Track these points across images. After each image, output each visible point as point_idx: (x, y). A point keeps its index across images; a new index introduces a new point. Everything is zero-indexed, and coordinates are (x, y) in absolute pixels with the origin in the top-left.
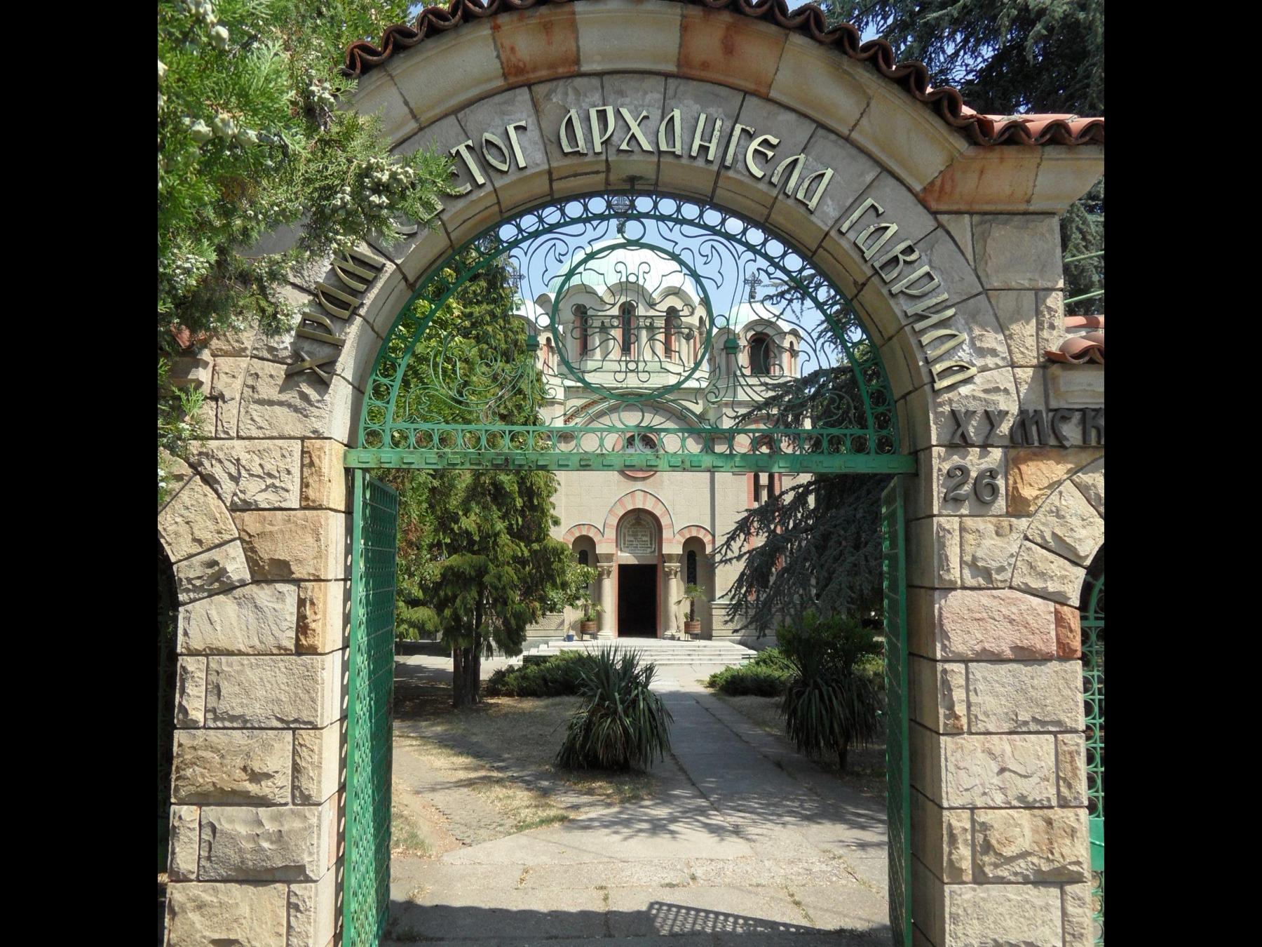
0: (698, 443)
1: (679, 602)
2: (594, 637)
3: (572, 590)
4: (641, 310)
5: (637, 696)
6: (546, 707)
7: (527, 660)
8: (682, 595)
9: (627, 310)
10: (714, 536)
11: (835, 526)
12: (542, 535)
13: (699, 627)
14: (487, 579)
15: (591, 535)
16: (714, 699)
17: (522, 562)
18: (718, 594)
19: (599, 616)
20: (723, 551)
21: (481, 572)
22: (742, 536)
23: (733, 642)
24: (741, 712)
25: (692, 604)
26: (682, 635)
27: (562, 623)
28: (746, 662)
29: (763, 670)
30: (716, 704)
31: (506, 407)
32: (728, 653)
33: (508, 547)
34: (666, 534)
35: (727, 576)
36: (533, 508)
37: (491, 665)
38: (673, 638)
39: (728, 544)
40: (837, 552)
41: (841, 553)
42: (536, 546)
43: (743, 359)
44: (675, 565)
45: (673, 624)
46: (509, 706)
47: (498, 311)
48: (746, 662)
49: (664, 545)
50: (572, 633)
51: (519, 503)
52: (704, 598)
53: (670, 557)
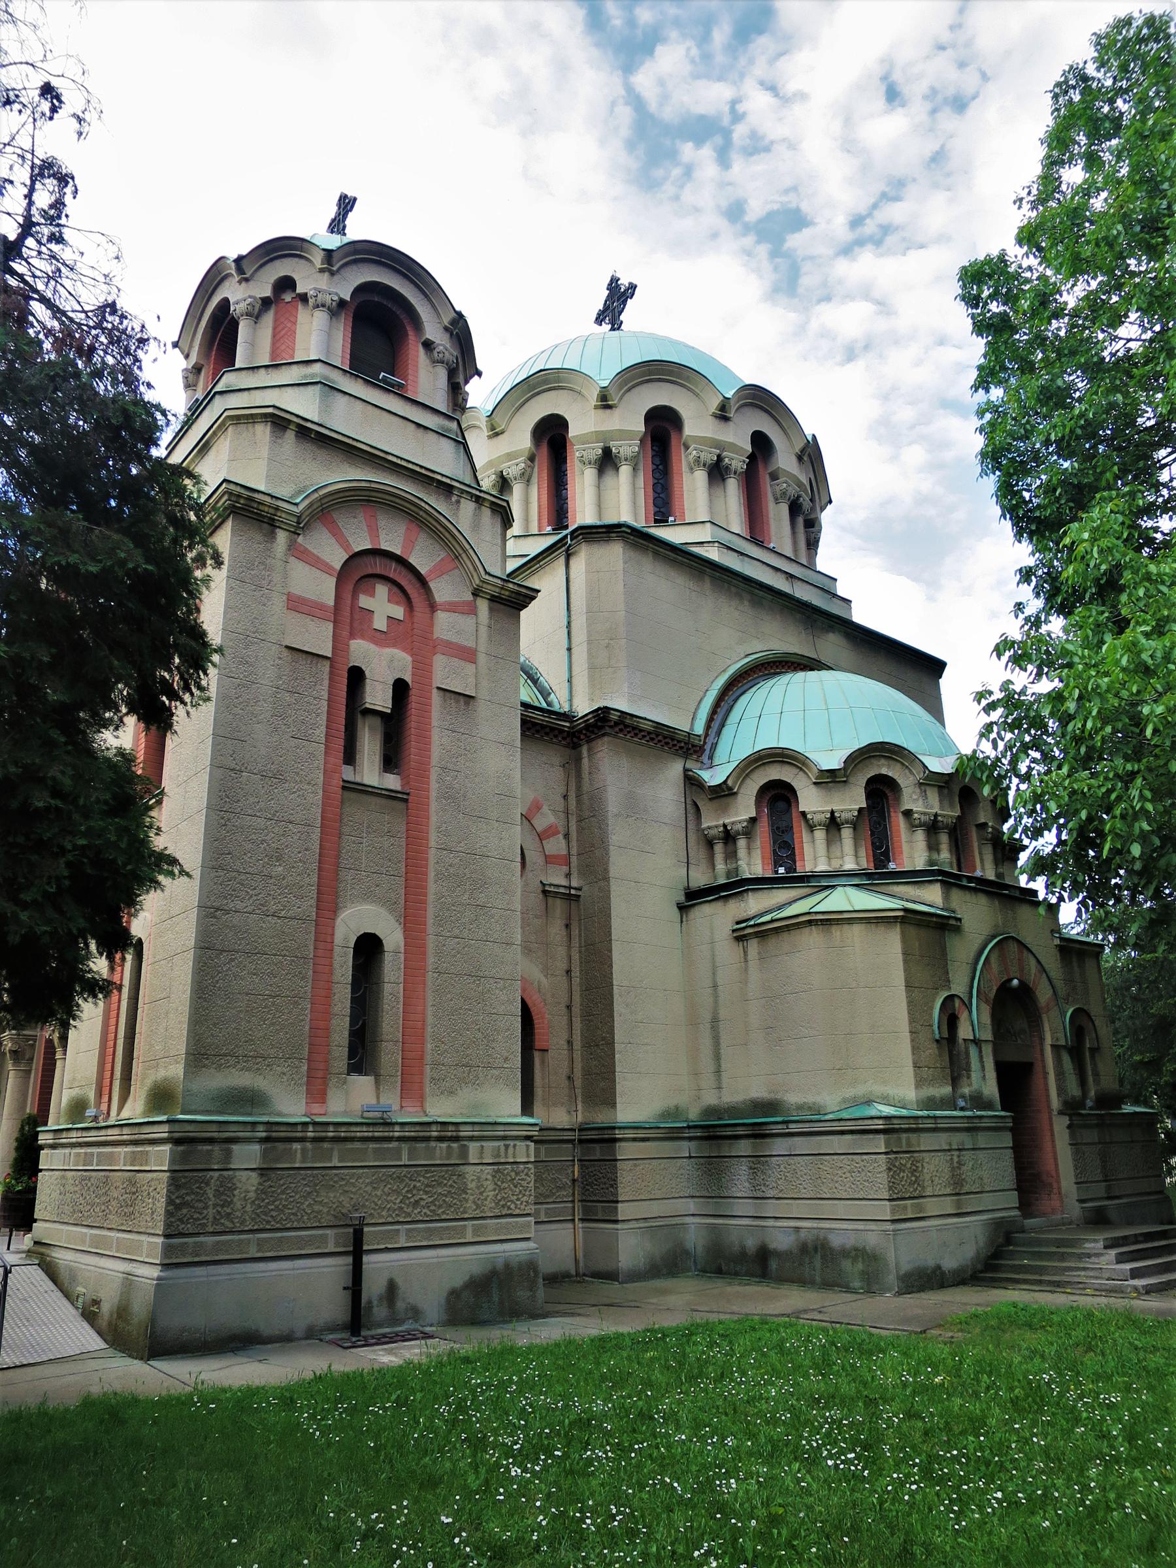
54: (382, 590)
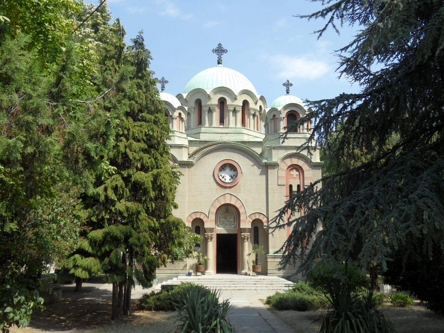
0: (259, 169)
1: (249, 254)
2: (203, 273)
3: (186, 247)
4: (229, 102)
5: (216, 325)
6: (169, 319)
7: (163, 287)
8: (251, 251)
9: (222, 102)
10: (268, 218)
11: (358, 201)
12: (167, 214)
13: (260, 268)
14: (131, 240)
15: (202, 218)
16: (269, 313)
17: (154, 230)
18: (271, 251)
19: (206, 262)
20: (277, 221)
21: (127, 237)
22: (289, 211)
23: (279, 276)
24: (286, 322)
25: (257, 255)
26: (251, 273)
27: (186, 266)
28: (287, 289)
29: (298, 295)
30: (270, 316)
31: (110, 102)
32: (276, 284)
33: (146, 221)
34: (242, 217)
35: (278, 239)
36: (163, 198)
37: (137, 292)
38: (246, 274)
39: (280, 216)
40: (363, 218)
41: (367, 219)
42: (162, 221)
43: (283, 124)
44: (247, 234)
45: (246, 266)
46: (147, 318)
47: (142, 83)
48: (287, 289)
49: (241, 223)
50: (191, 271)
51: (152, 194)
52: (263, 252)
53: (244, 230)
54: (294, 171)
